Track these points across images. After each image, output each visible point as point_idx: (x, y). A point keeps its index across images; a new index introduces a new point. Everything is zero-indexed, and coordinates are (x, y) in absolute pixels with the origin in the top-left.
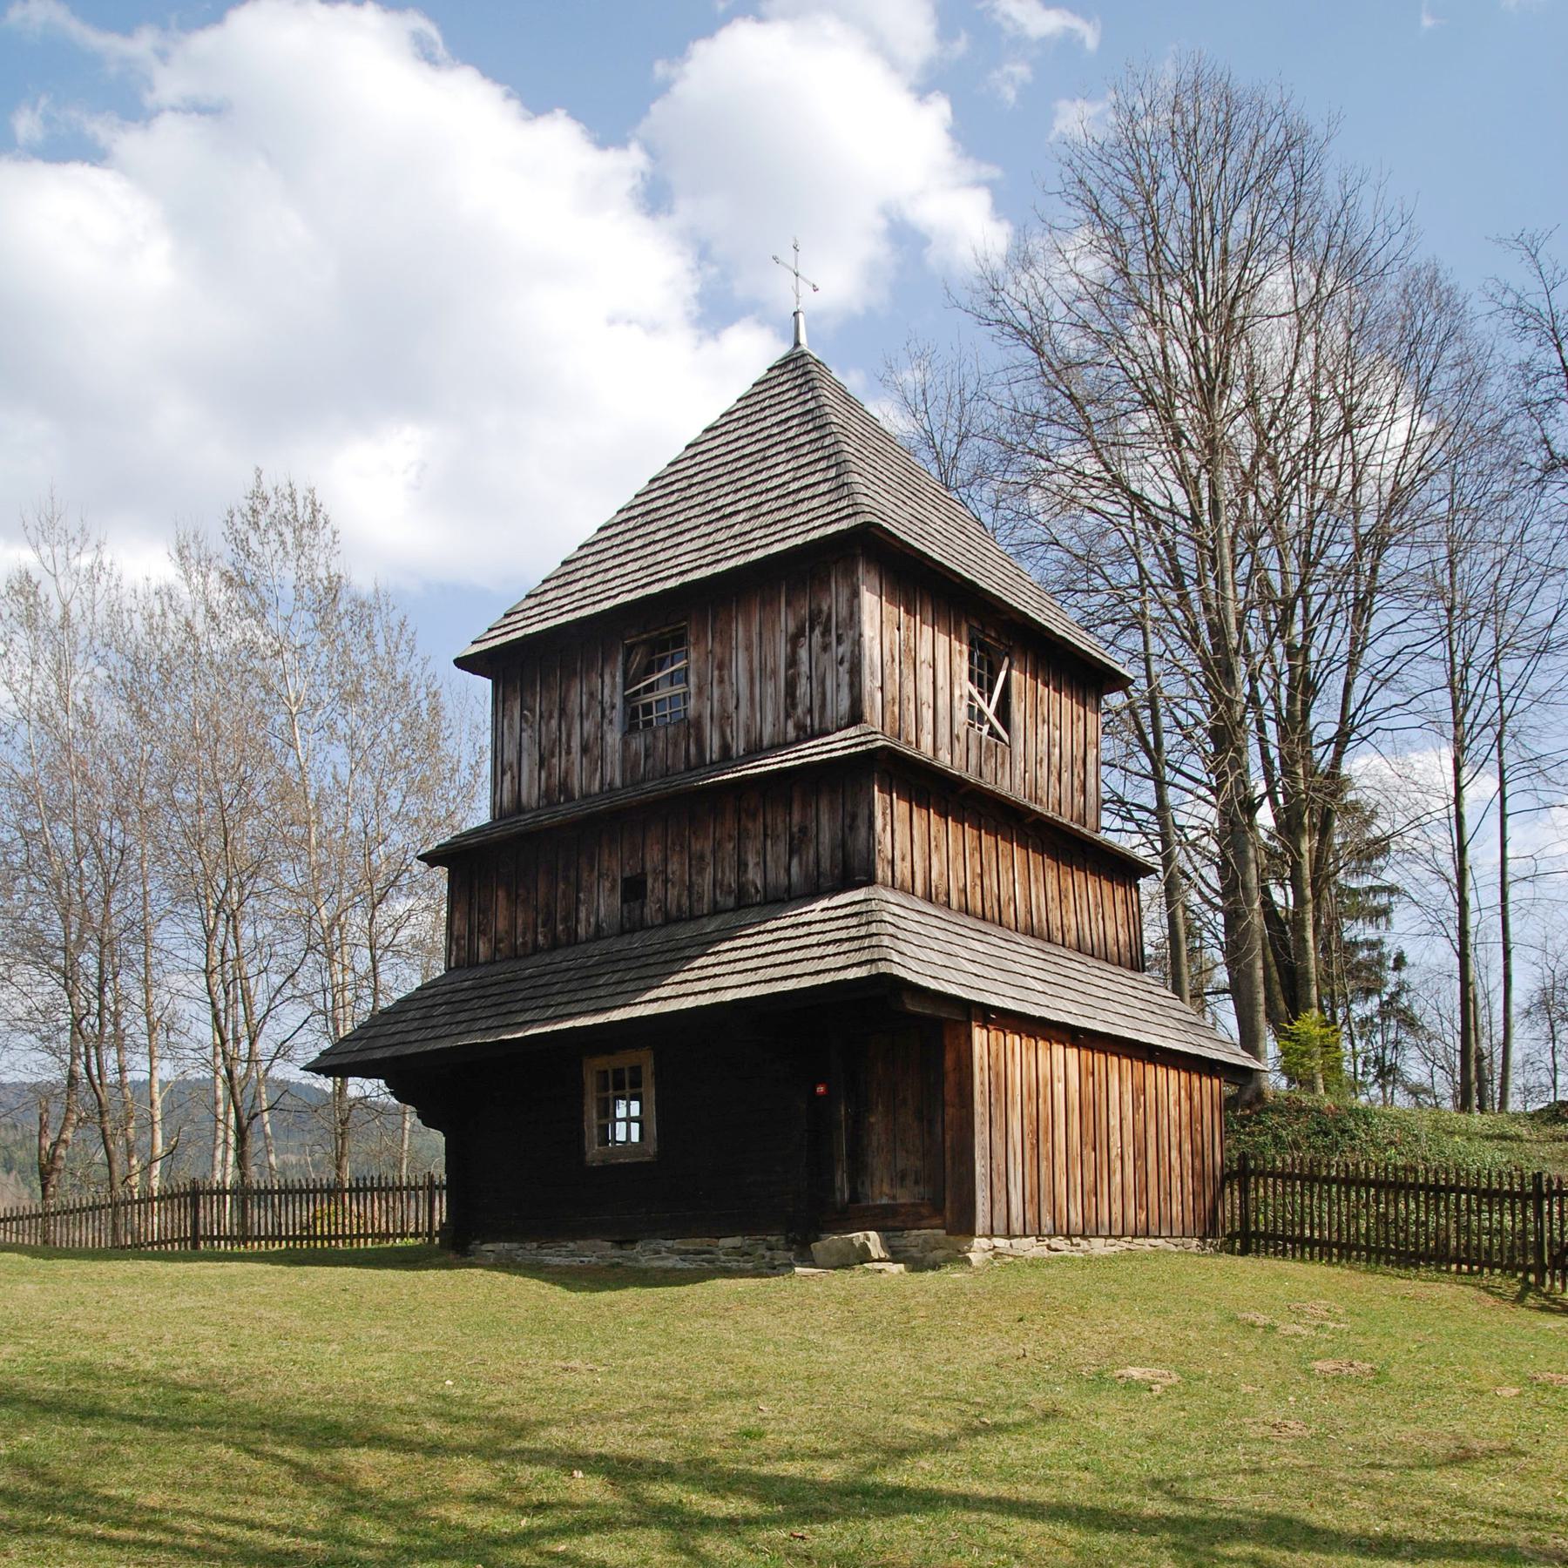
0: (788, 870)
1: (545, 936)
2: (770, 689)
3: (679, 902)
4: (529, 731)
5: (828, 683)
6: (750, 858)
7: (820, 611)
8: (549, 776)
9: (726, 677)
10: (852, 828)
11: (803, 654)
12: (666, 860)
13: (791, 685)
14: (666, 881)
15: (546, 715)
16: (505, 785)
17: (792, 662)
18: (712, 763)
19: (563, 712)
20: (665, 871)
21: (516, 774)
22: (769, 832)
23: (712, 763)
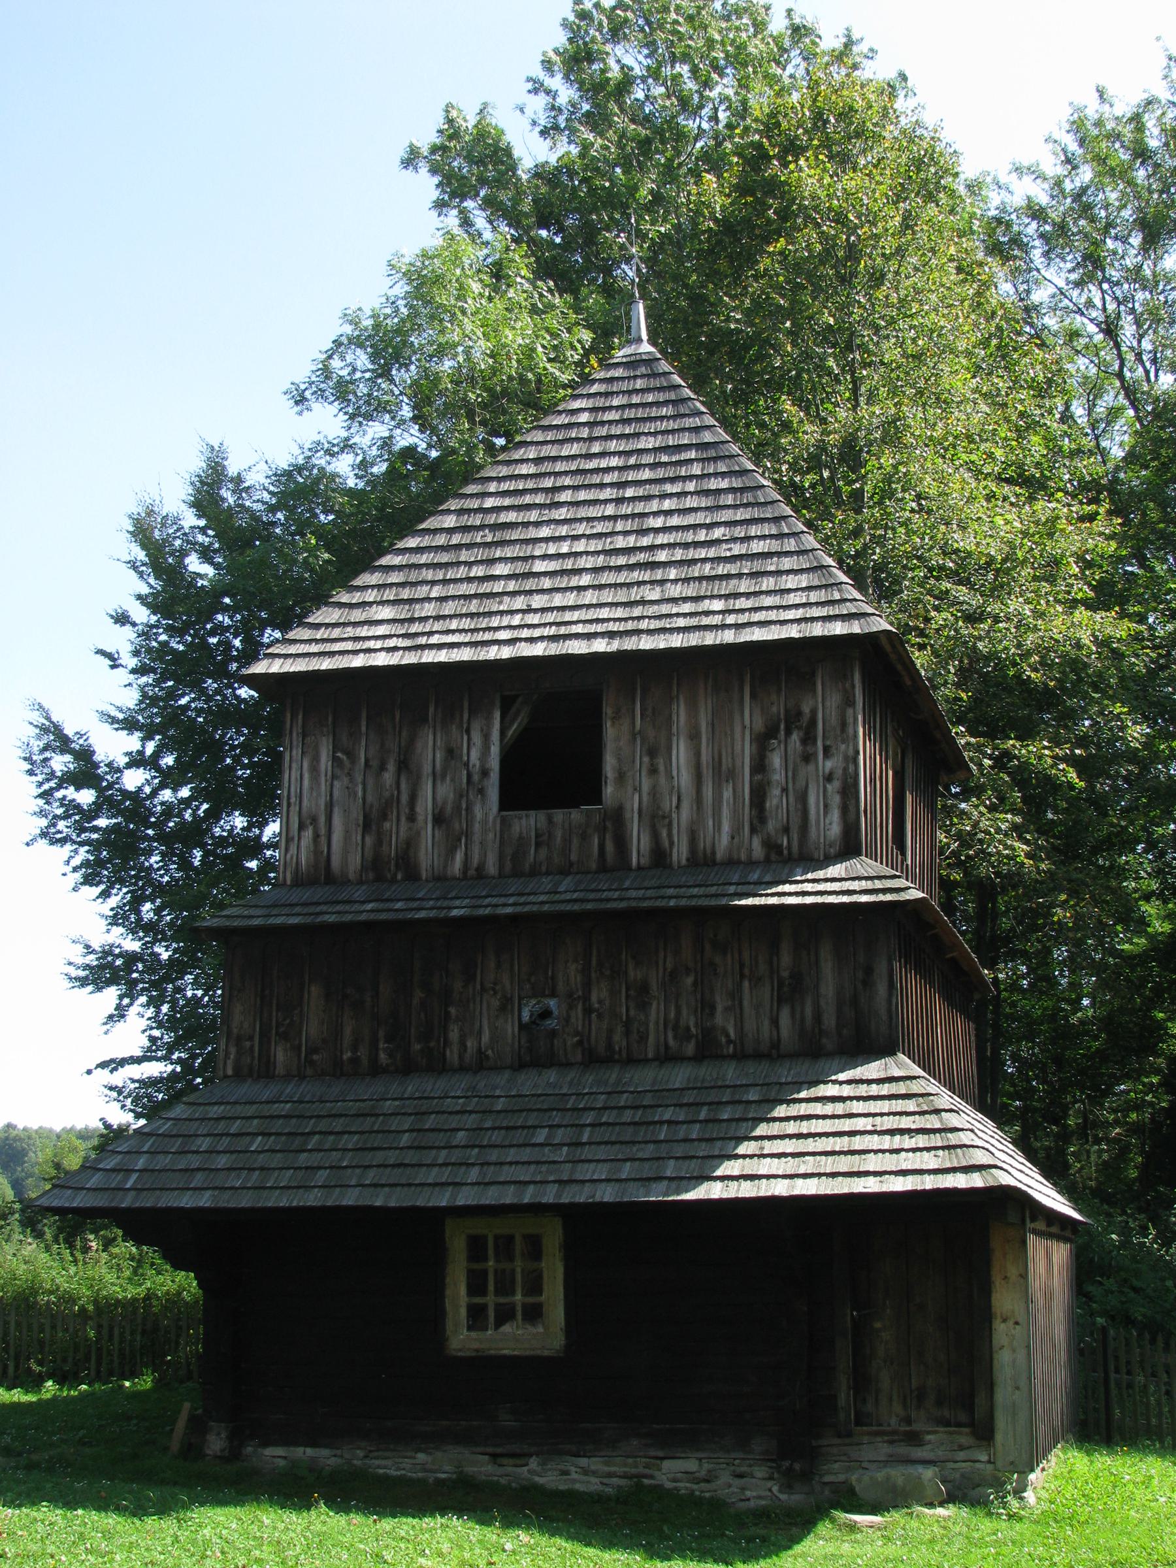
0: (775, 1022)
1: (391, 1056)
2: (727, 794)
3: (609, 1039)
4: (346, 780)
5: (812, 800)
6: (718, 998)
7: (799, 714)
8: (379, 843)
9: (662, 768)
10: (868, 982)
11: (776, 760)
12: (587, 985)
13: (759, 795)
14: (588, 1011)
15: (375, 763)
16: (304, 843)
17: (760, 766)
18: (639, 868)
19: (404, 765)
20: (586, 998)
21: (323, 831)
22: (746, 971)
23: (639, 868)
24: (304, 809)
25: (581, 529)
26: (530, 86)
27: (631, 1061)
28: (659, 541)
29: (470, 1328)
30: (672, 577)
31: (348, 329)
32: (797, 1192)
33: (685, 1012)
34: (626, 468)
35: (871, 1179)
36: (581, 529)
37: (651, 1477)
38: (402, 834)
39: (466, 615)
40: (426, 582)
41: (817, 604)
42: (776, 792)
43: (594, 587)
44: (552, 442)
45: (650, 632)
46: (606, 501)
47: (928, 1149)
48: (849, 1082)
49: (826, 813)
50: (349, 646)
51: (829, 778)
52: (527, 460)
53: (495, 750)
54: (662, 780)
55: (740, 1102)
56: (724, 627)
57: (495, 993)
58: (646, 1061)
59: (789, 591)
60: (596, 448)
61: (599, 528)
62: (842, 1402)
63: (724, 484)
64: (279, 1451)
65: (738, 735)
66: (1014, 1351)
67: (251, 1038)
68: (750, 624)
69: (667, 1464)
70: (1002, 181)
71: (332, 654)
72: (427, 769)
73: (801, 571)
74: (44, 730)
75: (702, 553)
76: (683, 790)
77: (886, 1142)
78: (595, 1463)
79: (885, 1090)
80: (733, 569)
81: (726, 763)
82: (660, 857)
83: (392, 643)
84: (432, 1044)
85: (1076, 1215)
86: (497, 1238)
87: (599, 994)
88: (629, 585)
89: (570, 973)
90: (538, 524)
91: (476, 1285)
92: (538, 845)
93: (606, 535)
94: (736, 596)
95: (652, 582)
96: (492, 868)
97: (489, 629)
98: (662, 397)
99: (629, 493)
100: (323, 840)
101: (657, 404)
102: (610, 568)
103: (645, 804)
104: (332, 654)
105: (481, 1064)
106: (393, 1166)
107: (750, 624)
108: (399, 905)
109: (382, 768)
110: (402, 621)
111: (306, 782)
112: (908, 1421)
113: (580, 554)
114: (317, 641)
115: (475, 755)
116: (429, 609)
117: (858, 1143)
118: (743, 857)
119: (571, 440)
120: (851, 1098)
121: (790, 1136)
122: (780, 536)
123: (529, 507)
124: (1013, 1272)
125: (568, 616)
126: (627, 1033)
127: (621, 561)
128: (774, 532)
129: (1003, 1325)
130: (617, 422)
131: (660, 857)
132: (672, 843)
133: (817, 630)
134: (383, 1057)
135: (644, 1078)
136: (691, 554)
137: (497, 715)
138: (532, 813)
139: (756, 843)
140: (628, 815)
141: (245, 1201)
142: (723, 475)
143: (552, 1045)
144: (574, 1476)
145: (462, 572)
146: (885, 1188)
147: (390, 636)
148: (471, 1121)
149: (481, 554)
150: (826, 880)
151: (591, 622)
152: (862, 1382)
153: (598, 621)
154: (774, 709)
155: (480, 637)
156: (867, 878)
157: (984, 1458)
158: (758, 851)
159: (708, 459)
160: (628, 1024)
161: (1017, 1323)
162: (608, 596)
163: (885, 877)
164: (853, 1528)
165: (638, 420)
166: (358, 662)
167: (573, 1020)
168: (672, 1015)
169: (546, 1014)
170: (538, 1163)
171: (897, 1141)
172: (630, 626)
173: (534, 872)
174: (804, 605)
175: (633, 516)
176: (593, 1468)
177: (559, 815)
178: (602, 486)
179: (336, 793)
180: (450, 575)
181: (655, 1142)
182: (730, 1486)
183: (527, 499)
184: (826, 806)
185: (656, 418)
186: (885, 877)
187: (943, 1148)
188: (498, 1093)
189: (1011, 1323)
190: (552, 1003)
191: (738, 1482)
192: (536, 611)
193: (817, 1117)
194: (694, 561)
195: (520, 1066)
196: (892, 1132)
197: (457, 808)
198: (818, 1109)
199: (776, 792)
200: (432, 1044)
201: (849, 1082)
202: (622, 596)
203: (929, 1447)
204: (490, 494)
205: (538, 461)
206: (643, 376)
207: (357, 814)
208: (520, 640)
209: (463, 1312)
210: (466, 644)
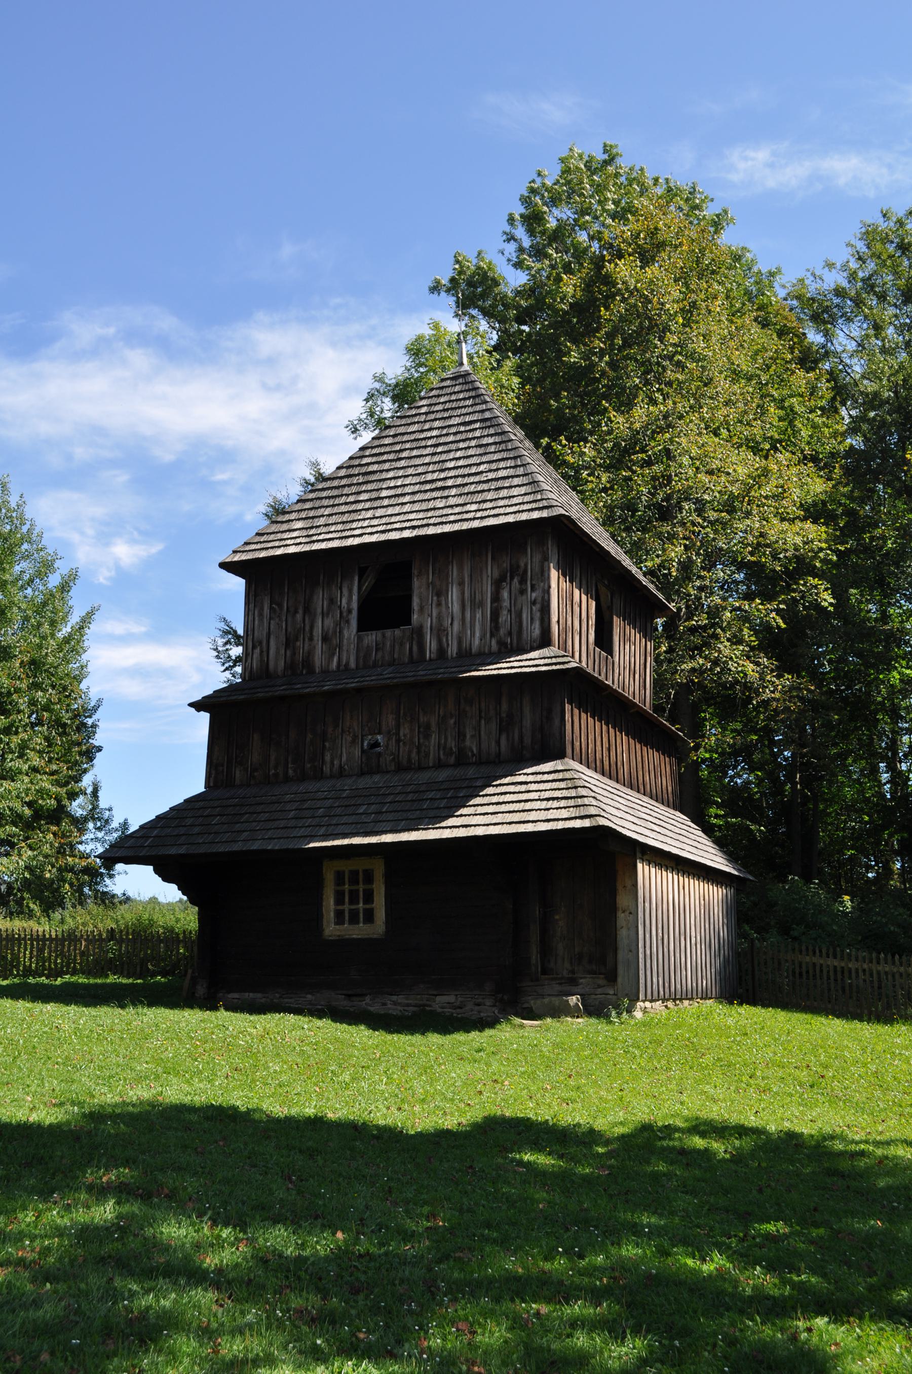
0: (498, 743)
2: (479, 615)
4: (277, 620)
5: (524, 616)
7: (518, 567)
8: (294, 654)
9: (443, 602)
11: (505, 594)
12: (398, 727)
14: (398, 741)
16: (255, 656)
17: (496, 598)
18: (430, 659)
20: (398, 734)
21: (265, 649)
22: (483, 714)
24: (255, 639)
25: (410, 471)
26: (505, 237)
27: (421, 768)
28: (450, 475)
29: (336, 923)
30: (453, 494)
31: (377, 385)
32: (488, 833)
33: (449, 739)
34: (441, 436)
35: (530, 824)
36: (410, 471)
37: (430, 1006)
38: (306, 648)
39: (340, 523)
40: (323, 507)
41: (527, 503)
42: (505, 612)
43: (410, 503)
44: (404, 425)
45: (435, 525)
46: (426, 455)
47: (565, 808)
48: (533, 774)
49: (532, 623)
50: (277, 544)
51: (534, 603)
52: (389, 436)
53: (355, 598)
54: (444, 609)
55: (471, 787)
56: (475, 519)
57: (350, 733)
58: (429, 768)
59: (514, 497)
60: (427, 426)
61: (420, 470)
62: (533, 961)
63: (491, 440)
64: (236, 995)
65: (484, 582)
66: (629, 929)
67: (223, 765)
68: (489, 516)
69: (438, 999)
70: (817, 274)
71: (267, 549)
72: (319, 610)
73: (523, 485)
74: (226, 633)
75: (472, 479)
76: (455, 615)
77: (544, 805)
78: (401, 999)
79: (551, 777)
80: (485, 487)
81: (478, 597)
82: (442, 652)
83: (298, 541)
84: (316, 764)
85: (736, 873)
86: (351, 872)
87: (405, 731)
88: (429, 500)
89: (389, 720)
90: (388, 471)
91: (339, 900)
92: (377, 650)
93: (423, 474)
94: (484, 501)
95: (441, 498)
96: (353, 665)
97: (351, 529)
98: (467, 395)
99: (440, 449)
100: (265, 654)
101: (464, 399)
102: (421, 492)
103: (434, 625)
104: (267, 549)
105: (341, 773)
106: (282, 828)
107: (489, 516)
108: (298, 686)
109: (296, 612)
110: (306, 529)
111: (256, 622)
112: (573, 972)
113: (407, 485)
114: (261, 542)
115: (344, 601)
116: (322, 521)
117: (528, 806)
118: (486, 651)
119: (414, 423)
120: (531, 782)
121: (493, 804)
122: (515, 467)
123: (385, 461)
124: (629, 883)
125: (393, 519)
126: (419, 752)
127: (428, 487)
128: (513, 465)
129: (623, 915)
130: (441, 411)
131: (442, 652)
132: (448, 645)
133: (524, 517)
134: (290, 772)
135: (424, 777)
136: (466, 480)
137: (356, 578)
138: (374, 632)
139: (494, 642)
140: (425, 631)
141: (202, 850)
142: (492, 435)
143: (379, 761)
144: (389, 1006)
145: (343, 500)
146: (536, 829)
147: (299, 537)
148: (328, 803)
149: (354, 489)
150: (526, 660)
151: (404, 521)
152: (546, 950)
153: (408, 521)
154: (505, 565)
155: (344, 534)
156: (548, 658)
157: (611, 992)
158: (494, 646)
159: (486, 428)
160: (419, 748)
161: (630, 913)
162: (416, 507)
163: (559, 657)
164: (522, 1026)
165: (452, 409)
166: (279, 552)
167: (390, 747)
168: (443, 741)
169: (376, 744)
170: (356, 823)
171: (550, 804)
172: (425, 522)
173: (375, 665)
174: (520, 504)
175: (439, 462)
176: (399, 1001)
177: (388, 633)
178: (426, 447)
179: (272, 627)
180: (337, 502)
181: (420, 810)
182: (472, 1010)
183: (385, 457)
184: (532, 619)
185: (462, 407)
186: (559, 657)
187: (573, 807)
188: (346, 788)
189: (627, 913)
190: (379, 737)
191: (477, 1008)
192: (377, 518)
193: (510, 793)
194: (466, 484)
195: (362, 774)
196: (548, 799)
197: (335, 632)
198: (512, 788)
199: (505, 612)
200: (316, 764)
201: (533, 774)
202: (424, 506)
203: (581, 986)
204: (366, 456)
205: (394, 436)
206: (460, 384)
207: (283, 639)
208: (365, 534)
209: (332, 914)
210: (336, 538)
